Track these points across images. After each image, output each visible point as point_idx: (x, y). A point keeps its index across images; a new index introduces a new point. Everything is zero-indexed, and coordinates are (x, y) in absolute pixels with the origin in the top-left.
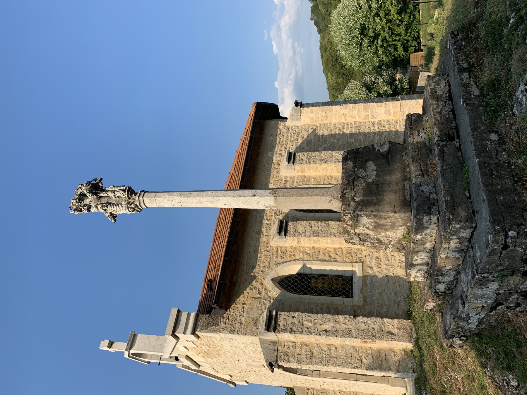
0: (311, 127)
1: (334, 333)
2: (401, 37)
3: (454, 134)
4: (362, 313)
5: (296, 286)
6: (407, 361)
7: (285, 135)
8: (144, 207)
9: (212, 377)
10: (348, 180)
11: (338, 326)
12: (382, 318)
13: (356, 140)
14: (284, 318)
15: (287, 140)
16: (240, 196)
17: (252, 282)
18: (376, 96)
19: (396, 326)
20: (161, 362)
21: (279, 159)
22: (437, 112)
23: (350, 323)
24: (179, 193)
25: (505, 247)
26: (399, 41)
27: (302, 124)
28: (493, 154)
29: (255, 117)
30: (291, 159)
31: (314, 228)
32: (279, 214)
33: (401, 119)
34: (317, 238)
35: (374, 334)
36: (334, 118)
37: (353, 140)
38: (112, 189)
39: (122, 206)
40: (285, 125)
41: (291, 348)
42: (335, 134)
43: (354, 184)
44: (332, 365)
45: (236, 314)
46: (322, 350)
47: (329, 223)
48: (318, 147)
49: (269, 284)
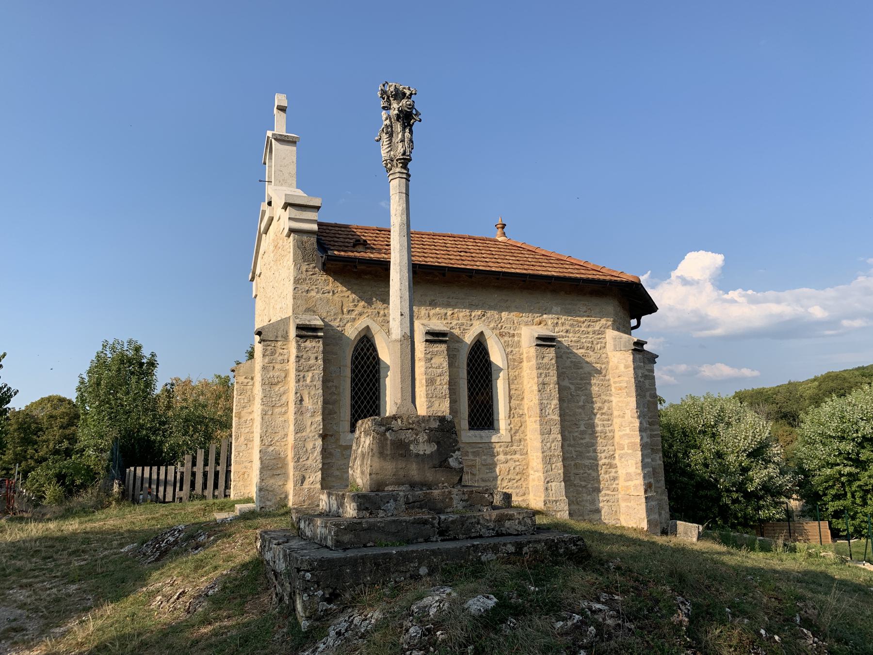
0: (603, 366)
2: (861, 506)
3: (448, 536)
5: (362, 358)
7: (590, 329)
9: (257, 249)
10: (413, 423)
11: (308, 415)
14: (315, 346)
16: (401, 297)
17: (362, 300)
18: (743, 464)
19: (312, 487)
21: (549, 323)
22: (479, 520)
23: (313, 431)
24: (405, 222)
26: (853, 503)
28: (402, 568)
30: (544, 341)
32: (462, 329)
33: (620, 496)
35: (301, 460)
36: (618, 399)
37: (582, 428)
39: (388, 152)
40: (607, 328)
41: (281, 357)
42: (593, 402)
43: (409, 429)
44: (263, 410)
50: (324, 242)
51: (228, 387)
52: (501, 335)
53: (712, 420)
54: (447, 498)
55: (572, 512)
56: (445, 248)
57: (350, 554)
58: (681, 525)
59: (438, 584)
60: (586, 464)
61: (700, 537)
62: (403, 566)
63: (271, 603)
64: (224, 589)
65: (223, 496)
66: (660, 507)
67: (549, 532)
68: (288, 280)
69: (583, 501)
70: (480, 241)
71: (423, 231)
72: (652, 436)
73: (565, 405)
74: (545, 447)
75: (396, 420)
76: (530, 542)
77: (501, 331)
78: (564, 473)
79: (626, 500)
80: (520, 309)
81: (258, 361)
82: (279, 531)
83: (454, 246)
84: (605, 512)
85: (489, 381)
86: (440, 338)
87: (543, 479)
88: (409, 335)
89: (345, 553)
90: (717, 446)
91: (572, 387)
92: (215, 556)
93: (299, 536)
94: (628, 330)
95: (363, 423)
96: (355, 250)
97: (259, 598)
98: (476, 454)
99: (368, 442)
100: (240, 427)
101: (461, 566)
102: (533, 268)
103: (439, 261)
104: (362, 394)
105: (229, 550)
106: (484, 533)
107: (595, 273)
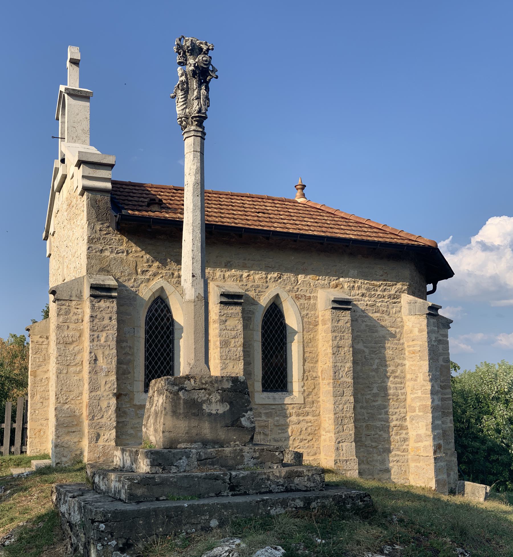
1: (93, 370)
3: (239, 491)
4: (125, 404)
5: (156, 319)
6: (69, 456)
8: (185, 136)
9: (50, 208)
10: (206, 383)
11: (103, 375)
12: (116, 427)
13: (375, 395)
15: (376, 296)
17: (157, 260)
19: (107, 444)
20: (60, 139)
21: (346, 286)
22: (269, 476)
24: (199, 182)
25: (93, 521)
27: (404, 318)
29: (419, 246)
31: (233, 341)
32: (257, 291)
33: (410, 457)
34: (219, 346)
35: (96, 418)
36: (411, 363)
37: (375, 391)
38: (201, 95)
39: (183, 110)
40: (403, 292)
41: (75, 317)
42: (386, 366)
43: (202, 389)
44: (58, 369)
45: (114, 243)
46: (75, 356)
47: (241, 361)
48: (364, 343)
49: (157, 283)
50: (117, 201)
51: (24, 346)
52: (297, 298)
53: (506, 387)
54: (238, 455)
55: (362, 471)
56: (242, 209)
57: (143, 506)
58: (469, 485)
59: (228, 536)
60: (378, 426)
61: (487, 497)
62: (194, 518)
63: (66, 553)
64: (20, 539)
65: (20, 452)
66: (449, 468)
67: (337, 488)
68: (82, 239)
69: (373, 460)
70: (279, 202)
71: (221, 190)
72: (443, 400)
73: (359, 368)
74: (337, 409)
75: (189, 380)
76: (318, 498)
77: (297, 293)
78: (355, 434)
79: (415, 460)
80: (318, 272)
81: (53, 321)
82: (74, 485)
83: (252, 206)
84: (395, 472)
85: (283, 344)
86: (235, 300)
87: (334, 439)
88: (203, 296)
89: (138, 506)
90: (510, 413)
91: (367, 351)
92: (11, 508)
93: (94, 490)
94: (423, 294)
95: (156, 383)
96: (149, 209)
97: (55, 548)
98: (269, 415)
99: (161, 401)
100: (36, 385)
101: (251, 519)
102: (331, 230)
103: (236, 221)
104: (156, 354)
105: (25, 503)
106: (274, 489)
107: (393, 236)
